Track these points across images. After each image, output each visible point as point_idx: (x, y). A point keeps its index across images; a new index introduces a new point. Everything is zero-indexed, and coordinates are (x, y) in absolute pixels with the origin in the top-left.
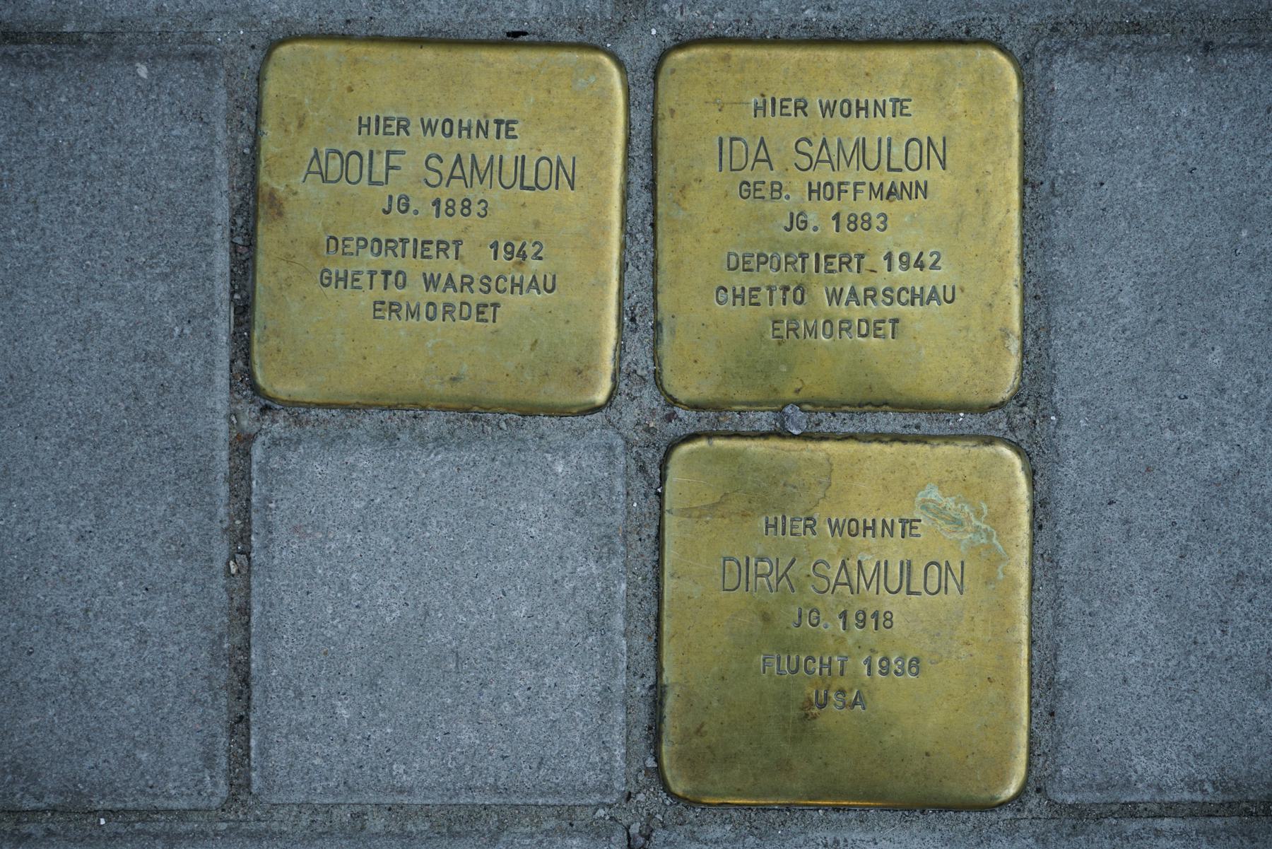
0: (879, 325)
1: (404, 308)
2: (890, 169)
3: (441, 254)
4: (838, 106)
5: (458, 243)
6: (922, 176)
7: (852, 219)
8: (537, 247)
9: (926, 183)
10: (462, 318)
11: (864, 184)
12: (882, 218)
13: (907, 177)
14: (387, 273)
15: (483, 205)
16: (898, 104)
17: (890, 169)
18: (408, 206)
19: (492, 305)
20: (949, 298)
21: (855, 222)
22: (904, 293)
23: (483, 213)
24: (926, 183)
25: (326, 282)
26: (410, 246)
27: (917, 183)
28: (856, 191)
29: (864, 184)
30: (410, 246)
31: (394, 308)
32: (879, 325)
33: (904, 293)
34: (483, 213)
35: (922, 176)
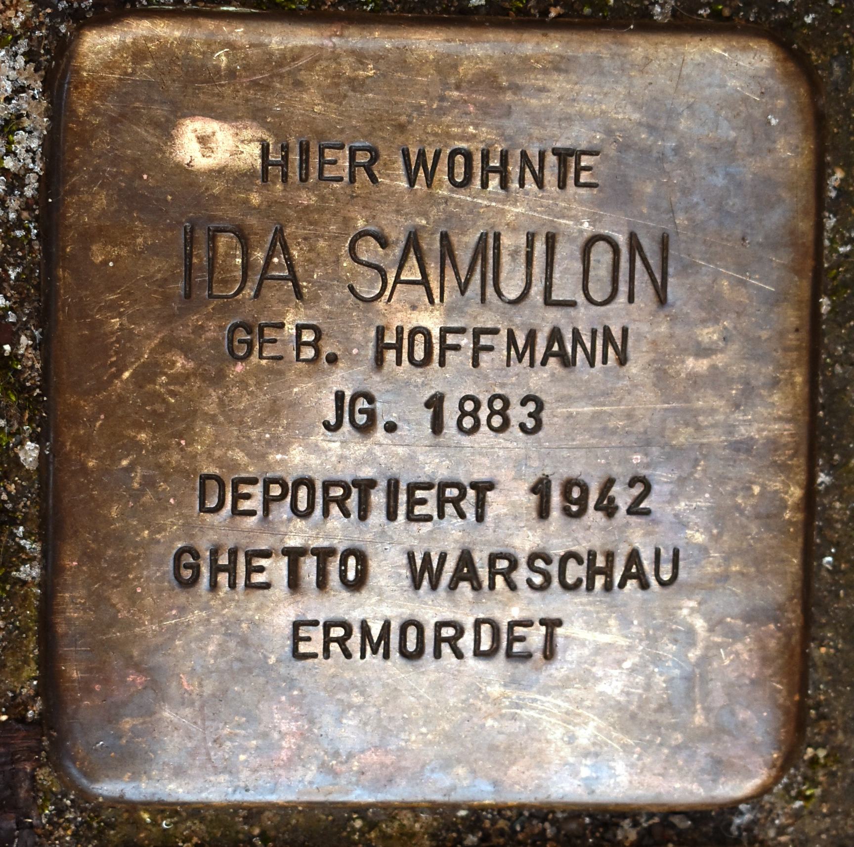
0: (519, 631)
1: (357, 635)
2: (548, 302)
3: (449, 509)
4: (443, 166)
5: (483, 488)
6: (616, 316)
7: (469, 406)
8: (638, 490)
9: (625, 331)
10: (478, 653)
11: (495, 331)
12: (531, 407)
13: (585, 318)
14: (323, 555)
15: (531, 407)
16: (572, 160)
17: (548, 302)
18: (372, 415)
19: (543, 622)
20: (666, 577)
21: (474, 414)
22: (572, 564)
23: (530, 424)
24: (625, 331)
25: (187, 574)
26: (378, 498)
27: (607, 331)
28: (478, 348)
29: (495, 331)
30: (378, 498)
31: (339, 635)
32: (519, 631)
33: (572, 564)
34: (530, 424)
35: (616, 316)
